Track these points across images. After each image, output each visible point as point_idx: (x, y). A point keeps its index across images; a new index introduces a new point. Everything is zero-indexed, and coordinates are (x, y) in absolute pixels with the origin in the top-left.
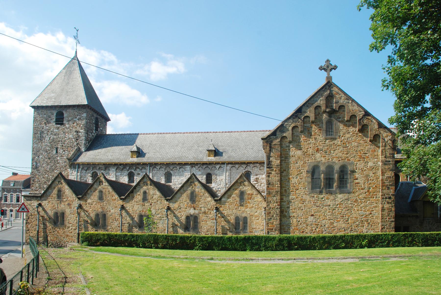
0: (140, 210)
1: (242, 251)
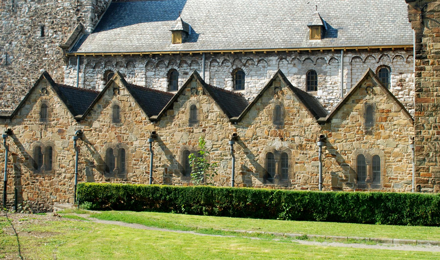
0: (185, 141)
1: (366, 223)
